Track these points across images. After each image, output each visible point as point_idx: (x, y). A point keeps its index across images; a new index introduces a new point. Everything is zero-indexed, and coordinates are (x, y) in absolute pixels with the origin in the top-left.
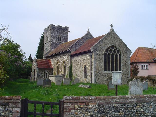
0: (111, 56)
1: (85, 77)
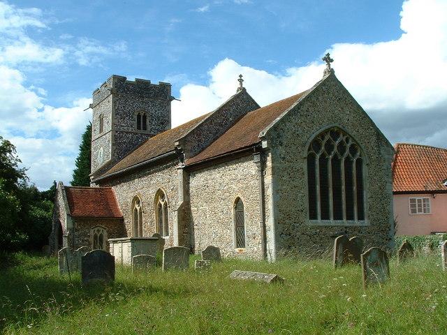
0: (330, 162)
1: (240, 242)
